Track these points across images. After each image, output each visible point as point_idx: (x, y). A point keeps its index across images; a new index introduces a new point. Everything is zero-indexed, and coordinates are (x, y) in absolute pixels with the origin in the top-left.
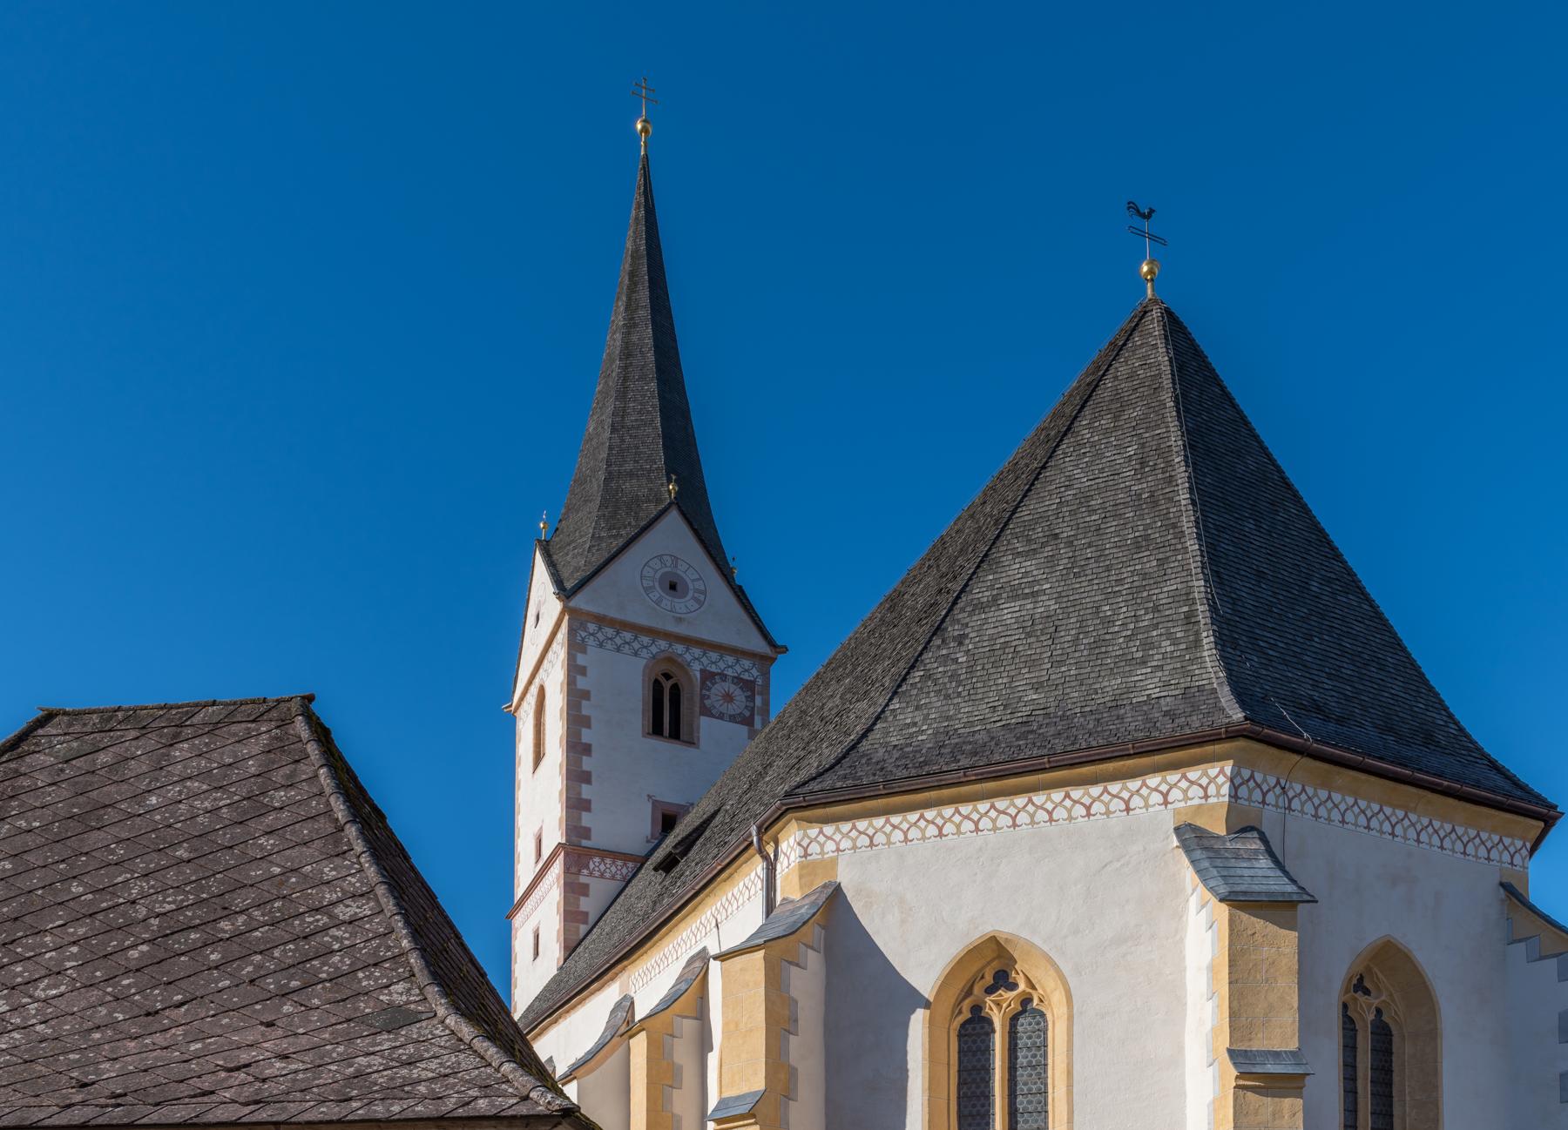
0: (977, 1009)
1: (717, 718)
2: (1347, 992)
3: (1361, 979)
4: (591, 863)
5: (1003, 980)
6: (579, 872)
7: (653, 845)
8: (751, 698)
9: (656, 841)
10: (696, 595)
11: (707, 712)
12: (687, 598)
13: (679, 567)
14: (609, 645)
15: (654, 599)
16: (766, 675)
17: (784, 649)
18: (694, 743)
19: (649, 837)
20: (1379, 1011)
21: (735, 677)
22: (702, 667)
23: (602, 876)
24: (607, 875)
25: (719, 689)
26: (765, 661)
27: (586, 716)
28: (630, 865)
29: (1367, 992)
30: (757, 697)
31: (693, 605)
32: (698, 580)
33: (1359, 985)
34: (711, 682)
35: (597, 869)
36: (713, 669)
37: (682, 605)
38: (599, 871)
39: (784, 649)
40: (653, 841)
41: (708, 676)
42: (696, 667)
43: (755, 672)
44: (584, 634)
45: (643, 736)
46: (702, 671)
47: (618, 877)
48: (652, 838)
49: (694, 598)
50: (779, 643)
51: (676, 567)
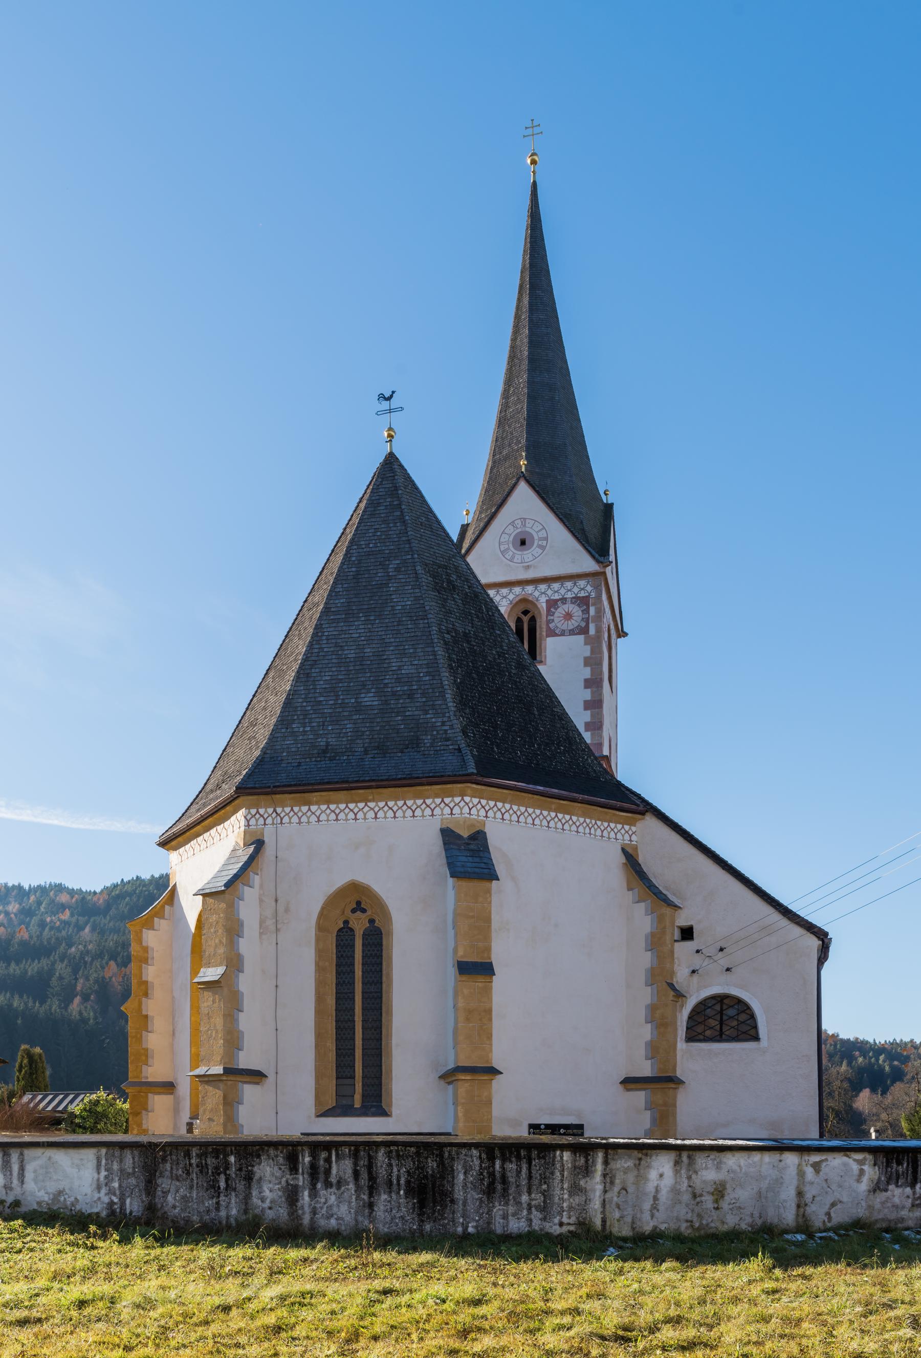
0: (346, 922)
1: (560, 636)
10: (540, 543)
11: (552, 633)
21: (573, 598)
30: (591, 608)
49: (540, 546)
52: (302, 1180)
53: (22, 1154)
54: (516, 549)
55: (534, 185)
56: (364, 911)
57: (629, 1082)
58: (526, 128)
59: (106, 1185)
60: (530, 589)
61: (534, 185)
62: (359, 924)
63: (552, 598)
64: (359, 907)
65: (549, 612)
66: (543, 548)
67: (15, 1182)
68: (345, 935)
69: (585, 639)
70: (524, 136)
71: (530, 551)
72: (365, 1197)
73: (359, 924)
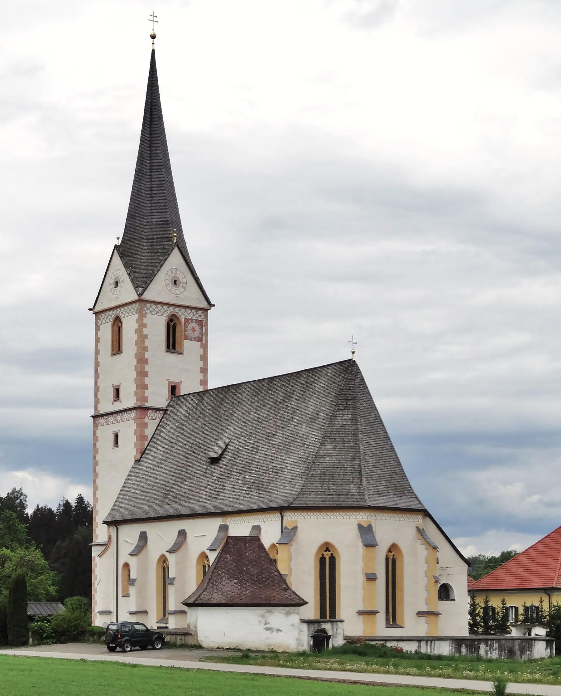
0: (323, 555)
1: (190, 340)
2: (387, 553)
3: (390, 549)
4: (148, 413)
5: (327, 550)
6: (144, 418)
7: (169, 402)
8: (201, 329)
9: (170, 400)
10: (183, 285)
11: (186, 338)
12: (180, 287)
13: (177, 273)
14: (154, 313)
15: (166, 284)
16: (206, 316)
17: (214, 306)
18: (182, 353)
19: (167, 398)
20: (393, 556)
21: (196, 320)
22: (185, 317)
23: (152, 419)
24: (154, 418)
25: (192, 325)
26: (206, 310)
27: (146, 346)
28: (161, 412)
29: (391, 552)
30: (203, 327)
31: (182, 289)
32: (184, 277)
33: (390, 551)
34: (188, 324)
35: (150, 416)
36: (189, 317)
37: (178, 290)
38: (151, 416)
39: (214, 306)
40: (168, 400)
41: (187, 321)
42: (183, 317)
43: (203, 316)
44: (146, 309)
45: (165, 353)
46: (185, 319)
47: (157, 418)
48: (168, 399)
49: (183, 287)
50: (212, 303)
51: (176, 273)
52: (488, 648)
53: (434, 642)
54: (172, 285)
55: (153, 51)
56: (329, 551)
57: (342, 621)
58: (157, 22)
59: (451, 651)
60: (177, 309)
61: (153, 51)
62: (327, 555)
63: (187, 317)
64: (327, 550)
65: (185, 326)
66: (185, 288)
67: (433, 650)
68: (322, 560)
69: (201, 344)
70: (149, 20)
71: (178, 288)
72: (500, 653)
73: (327, 555)
